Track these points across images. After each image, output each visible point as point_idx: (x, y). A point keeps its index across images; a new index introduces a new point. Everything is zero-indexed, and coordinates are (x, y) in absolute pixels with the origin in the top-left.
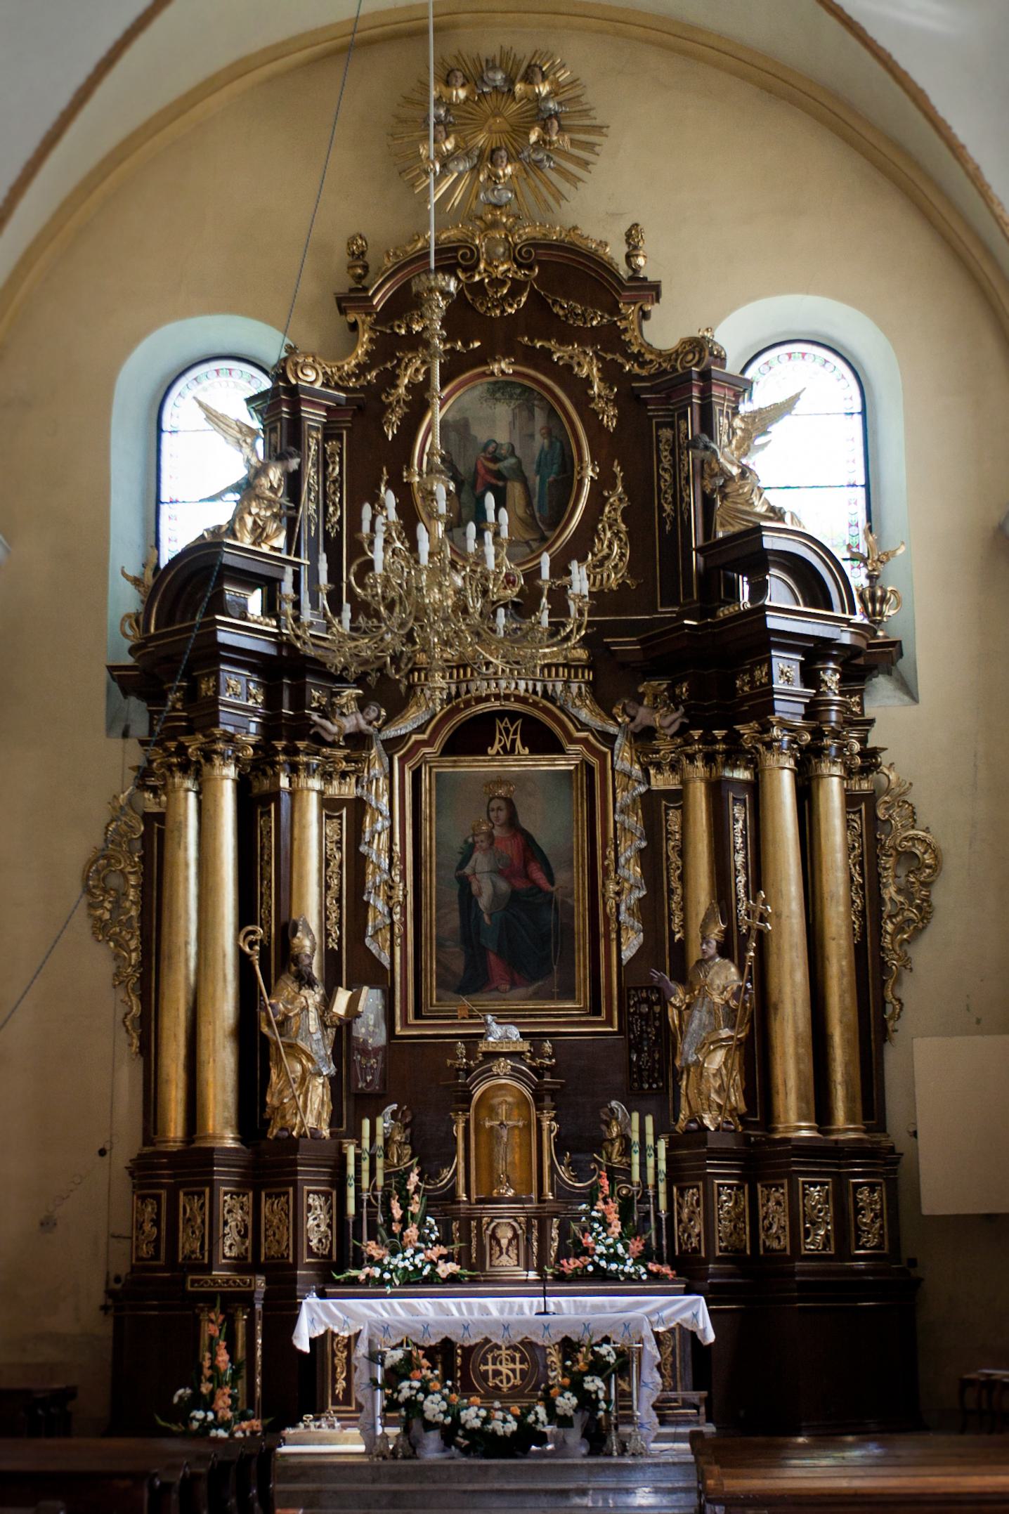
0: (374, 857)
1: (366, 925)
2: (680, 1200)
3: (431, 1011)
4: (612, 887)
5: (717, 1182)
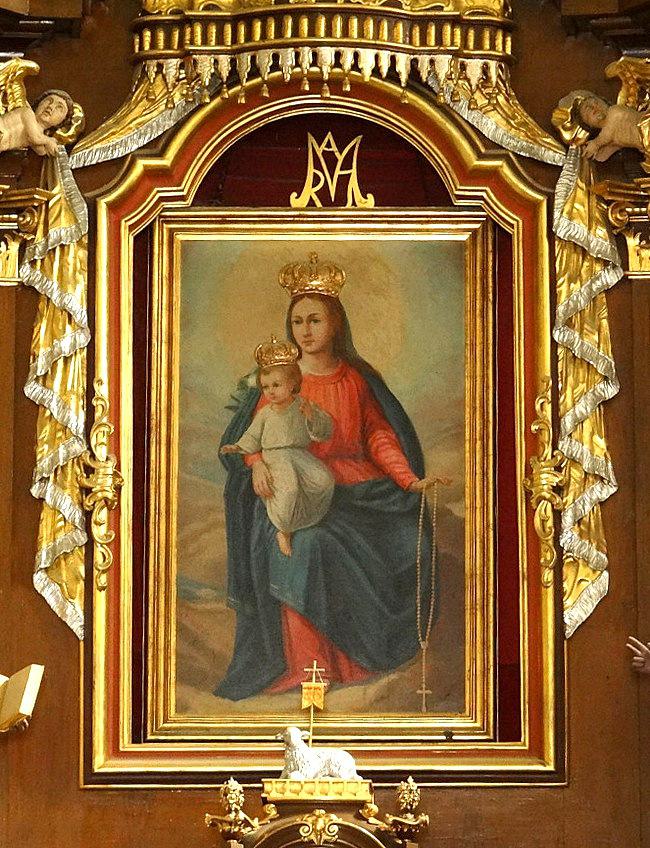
0: (54, 408)
1: (34, 549)
3: (167, 731)
4: (547, 479)
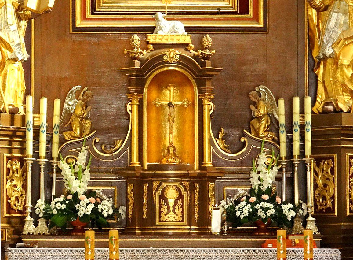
2: (317, 169)
5: (349, 154)
